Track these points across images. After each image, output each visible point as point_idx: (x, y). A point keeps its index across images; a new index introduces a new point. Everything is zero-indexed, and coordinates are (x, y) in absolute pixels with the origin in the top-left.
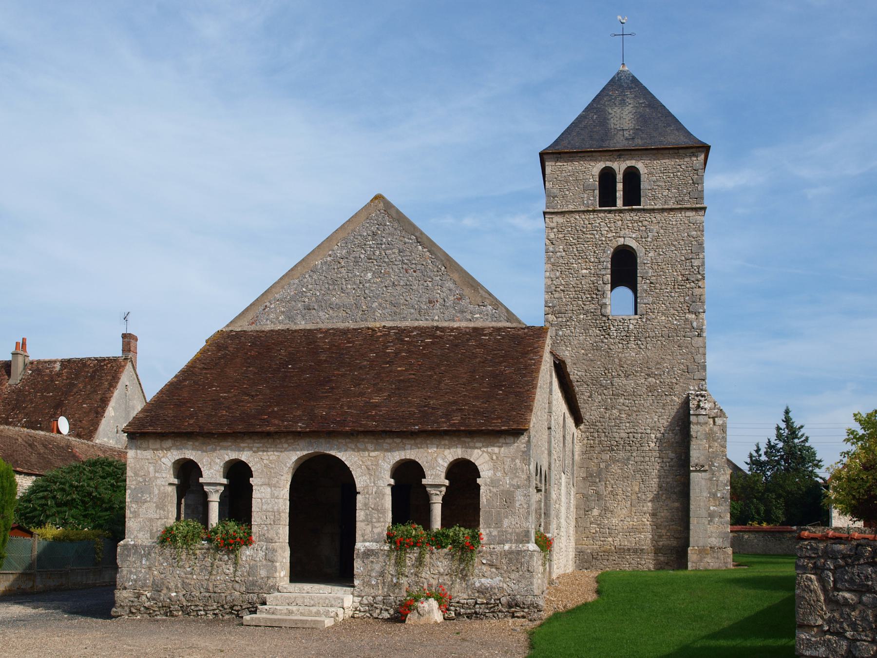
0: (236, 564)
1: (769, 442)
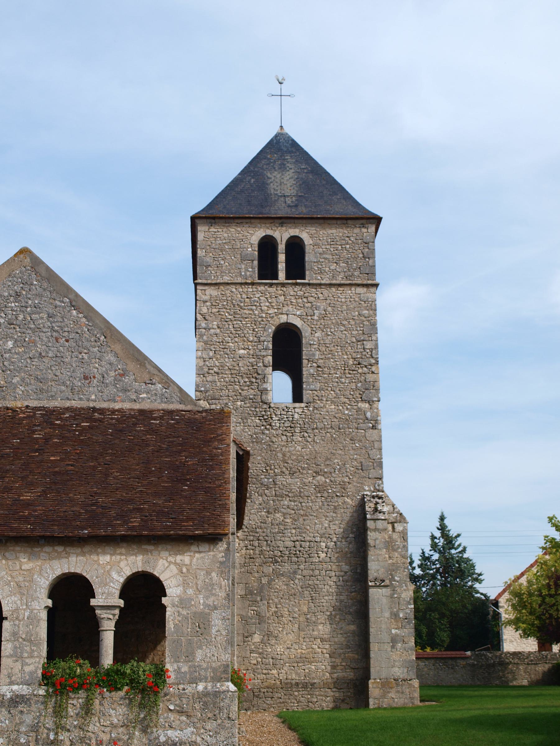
1: (423, 553)
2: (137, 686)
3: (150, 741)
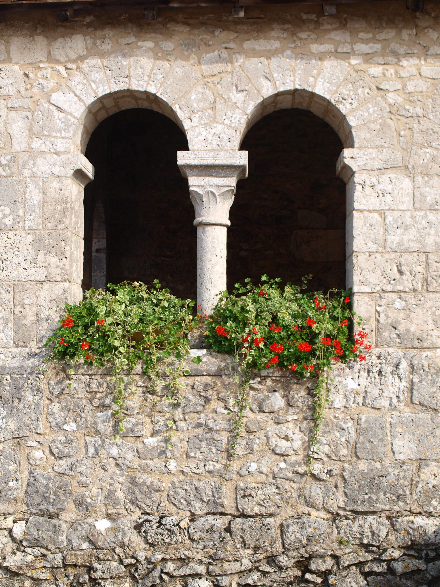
0: (313, 415)
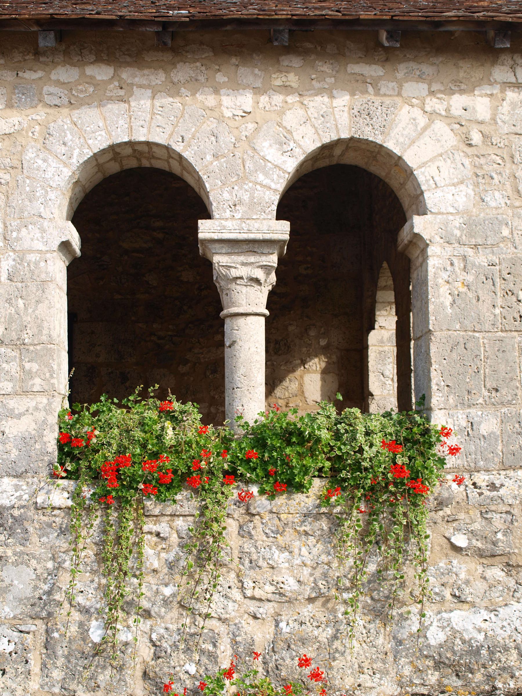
2: (355, 479)
3: (400, 642)
